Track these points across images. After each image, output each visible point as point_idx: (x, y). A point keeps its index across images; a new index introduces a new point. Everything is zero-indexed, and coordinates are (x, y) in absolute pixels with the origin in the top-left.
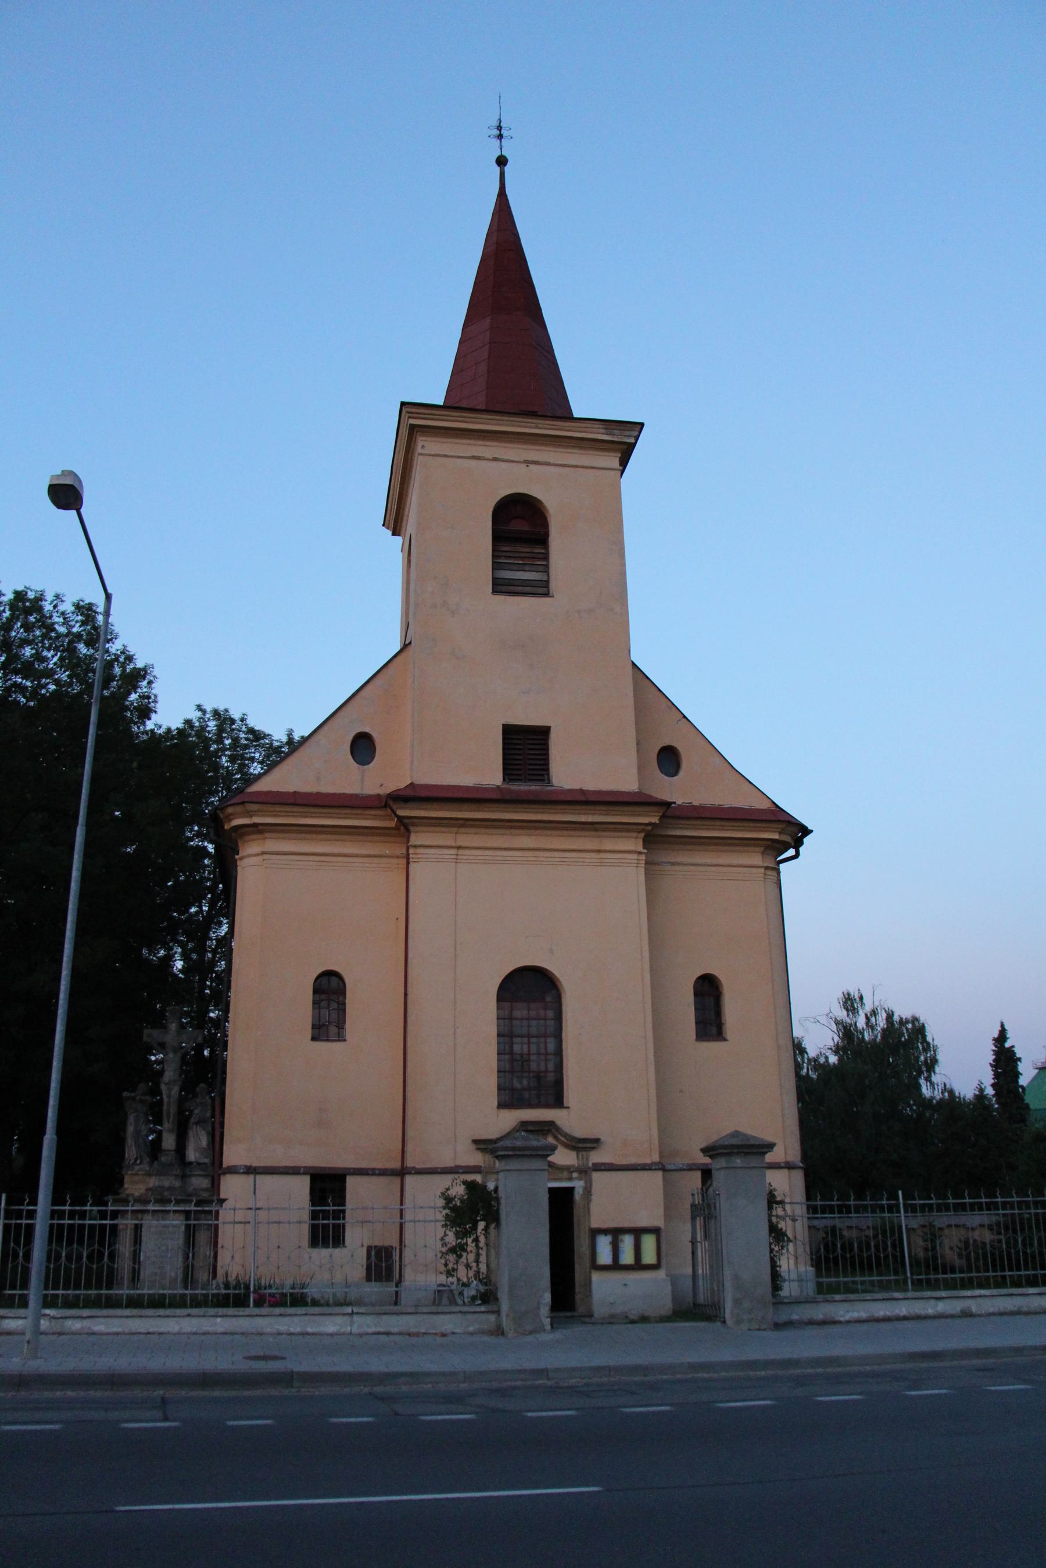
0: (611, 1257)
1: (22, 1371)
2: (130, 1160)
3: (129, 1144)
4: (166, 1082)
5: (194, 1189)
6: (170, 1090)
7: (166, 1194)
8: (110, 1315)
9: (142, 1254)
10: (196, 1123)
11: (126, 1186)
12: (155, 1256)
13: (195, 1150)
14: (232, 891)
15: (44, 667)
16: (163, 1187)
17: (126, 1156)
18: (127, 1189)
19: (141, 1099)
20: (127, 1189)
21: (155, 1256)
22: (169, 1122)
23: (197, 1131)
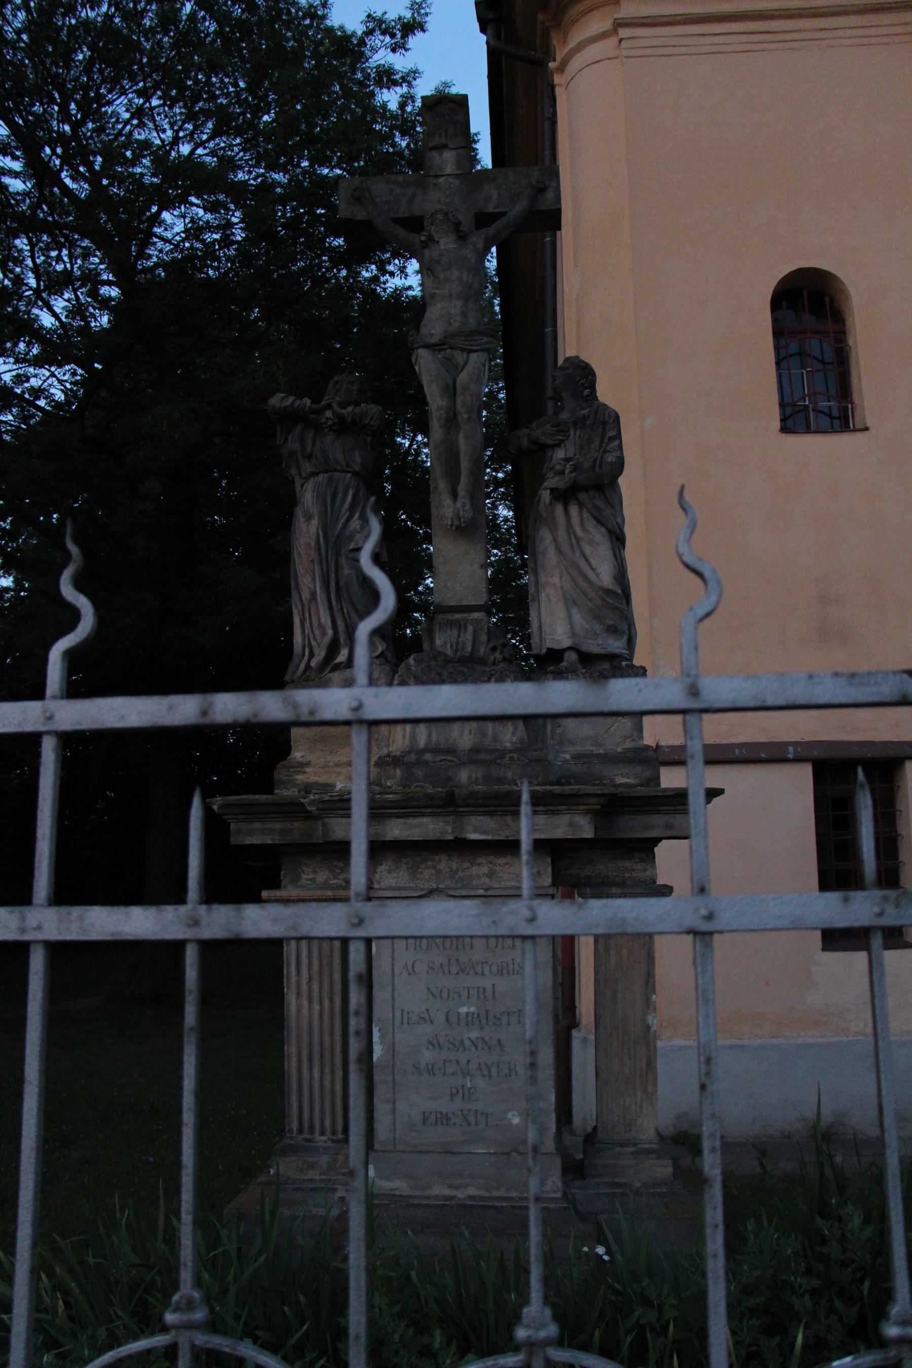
0: (100, 938)
1: (863, 409)
2: (312, 655)
3: (306, 595)
4: (435, 340)
5: (578, 757)
6: (453, 369)
7: (463, 775)
8: (794, 39)
9: (375, 1030)
10: (564, 496)
11: (297, 755)
12: (433, 1044)
13: (569, 603)
14: (547, 152)
15: (200, 108)
16: (450, 751)
17: (298, 638)
18: (302, 766)
19: (341, 418)
20: (302, 766)
21: (433, 1044)
22: (455, 496)
23: (569, 528)
